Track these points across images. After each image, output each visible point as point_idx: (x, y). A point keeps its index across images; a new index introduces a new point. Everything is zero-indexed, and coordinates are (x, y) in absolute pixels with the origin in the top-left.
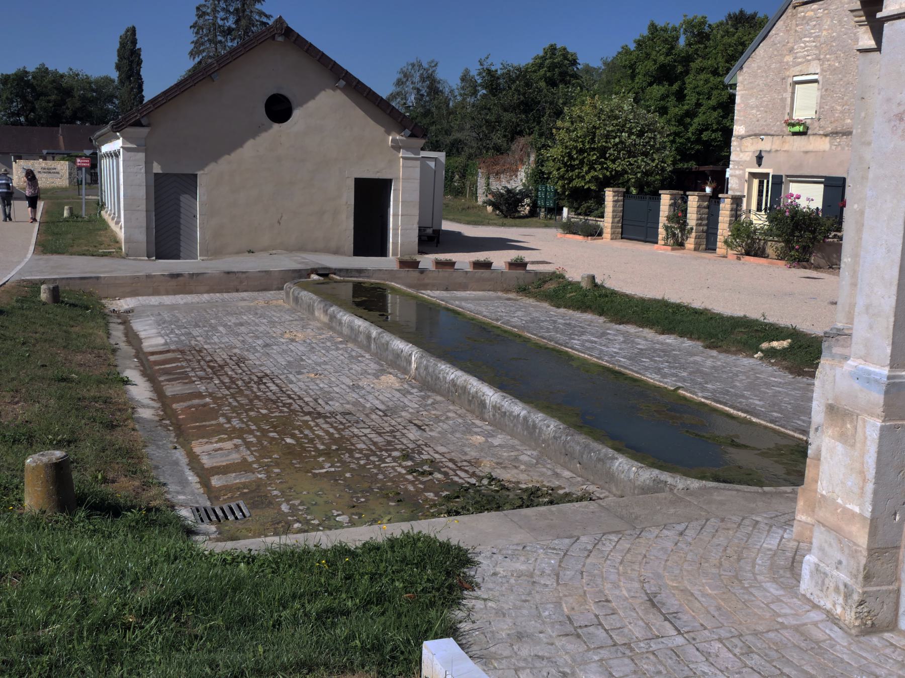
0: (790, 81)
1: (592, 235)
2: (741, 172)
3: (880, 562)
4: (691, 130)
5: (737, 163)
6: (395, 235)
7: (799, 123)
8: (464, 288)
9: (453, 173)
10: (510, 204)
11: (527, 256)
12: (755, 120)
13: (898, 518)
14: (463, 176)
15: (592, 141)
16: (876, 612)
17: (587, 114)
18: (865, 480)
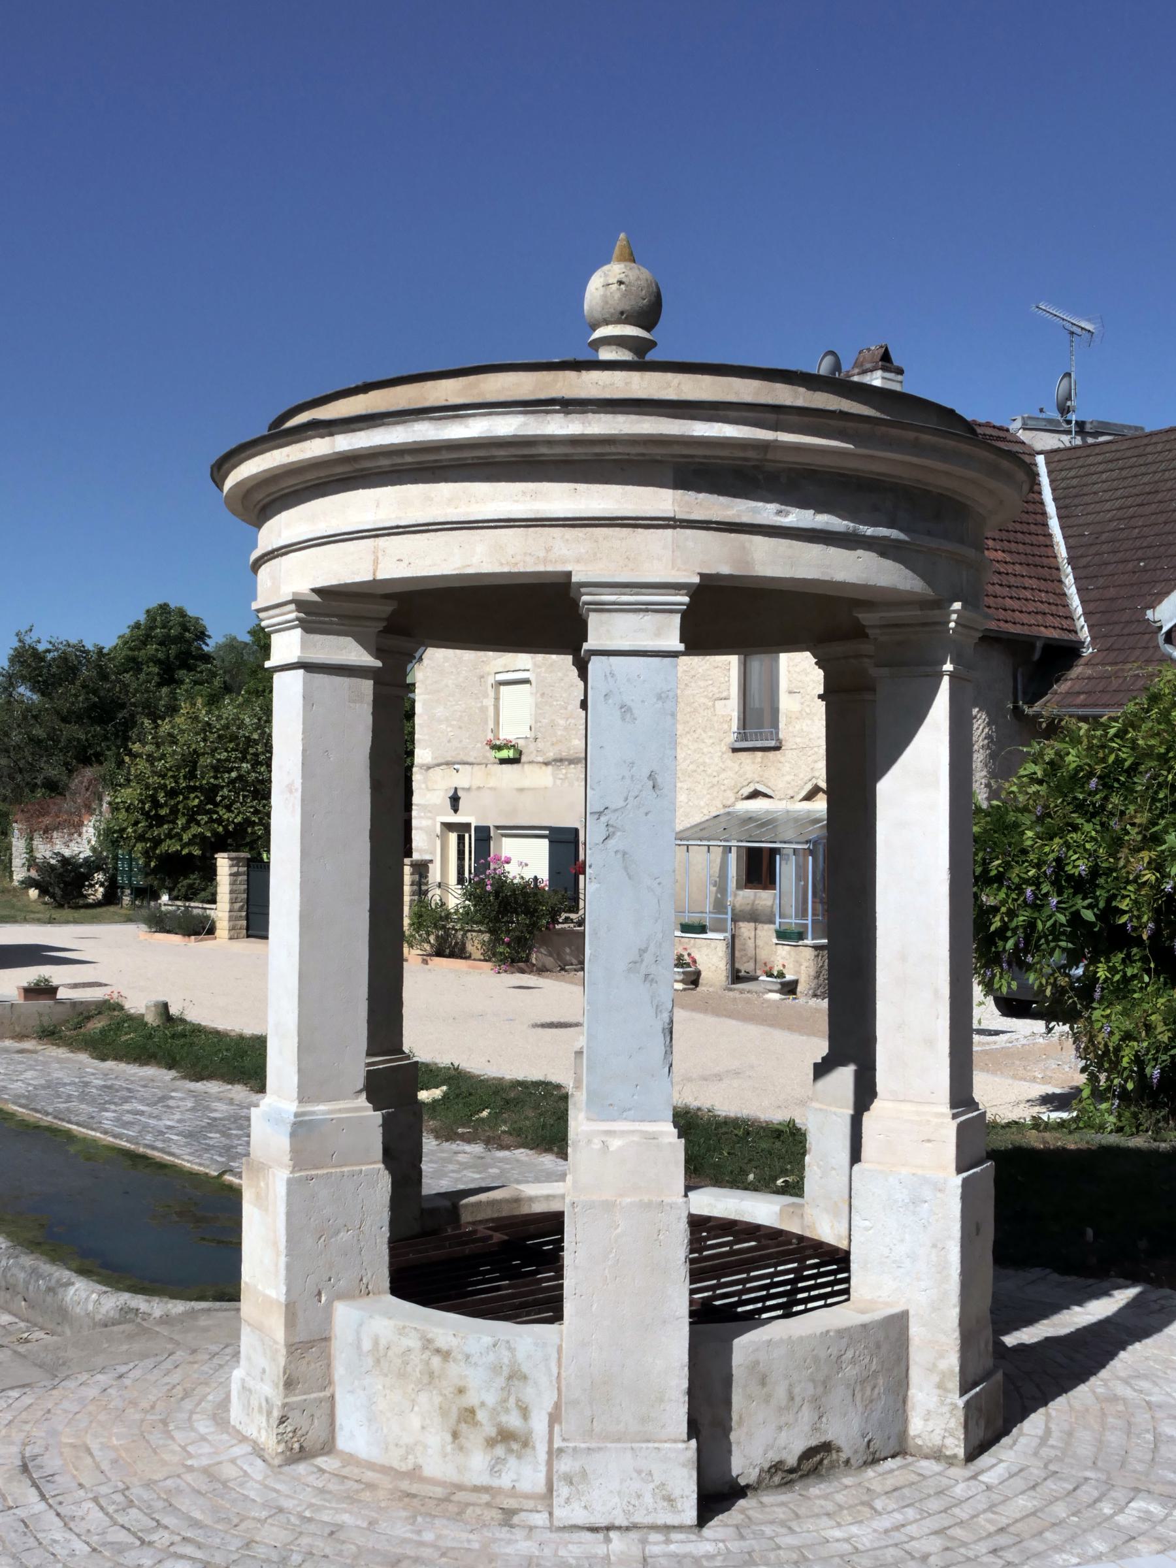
0: (491, 680)
1: (196, 933)
2: (429, 822)
3: (304, 1362)
7: (507, 746)
10: (66, 884)
11: (55, 974)
13: (323, 1299)
15: (191, 775)
16: (303, 1431)
17: (182, 731)
18: (278, 1255)
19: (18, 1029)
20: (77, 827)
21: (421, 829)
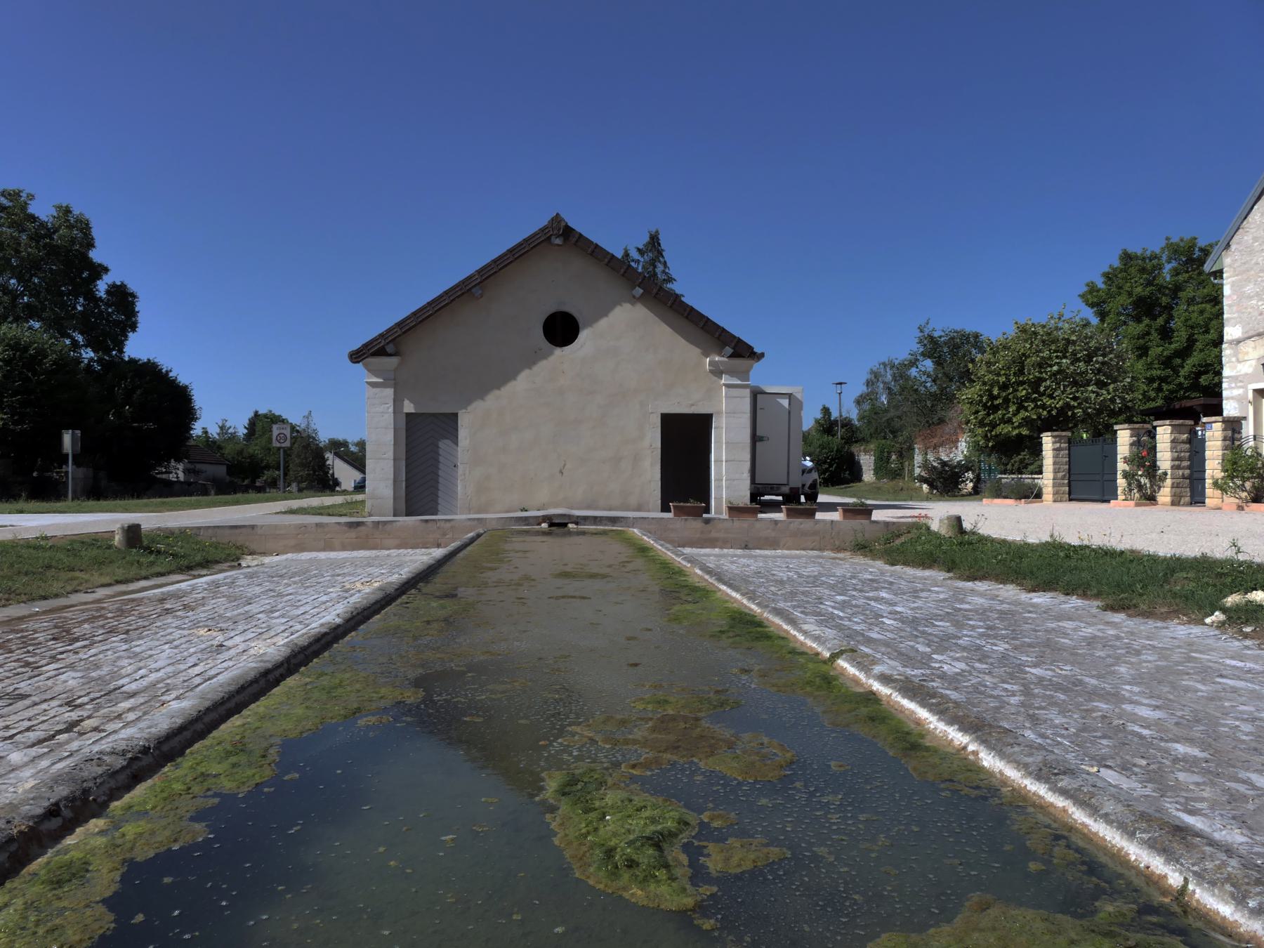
1: (1027, 497)
2: (1241, 391)
4: (1182, 373)
5: (1234, 379)
6: (719, 487)
8: (773, 544)
9: (889, 453)
12: (1256, 313)
14: (901, 455)
15: (1021, 372)
20: (955, 443)
21: (1232, 398)
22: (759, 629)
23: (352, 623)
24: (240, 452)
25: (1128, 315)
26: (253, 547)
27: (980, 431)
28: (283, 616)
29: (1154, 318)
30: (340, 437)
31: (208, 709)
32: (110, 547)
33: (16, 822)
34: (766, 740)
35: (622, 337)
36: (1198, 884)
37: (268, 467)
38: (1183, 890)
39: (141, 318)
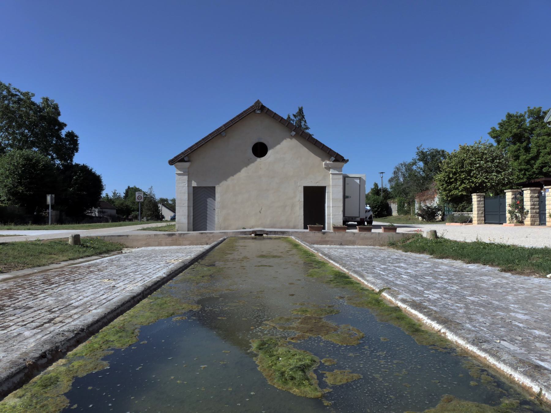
1: (465, 222)
4: (535, 167)
6: (329, 218)
8: (353, 243)
9: (404, 203)
10: (429, 215)
14: (409, 204)
15: (462, 167)
19: (381, 242)
20: (433, 199)
22: (348, 279)
23: (170, 277)
24: (122, 204)
25: (510, 141)
26: (127, 244)
27: (444, 193)
28: (140, 274)
29: (522, 143)
30: (164, 197)
31: (109, 313)
32: (67, 244)
33: (28, 360)
34: (351, 328)
35: (286, 153)
36: (547, 391)
37: (134, 211)
38: (540, 394)
39: (81, 146)
